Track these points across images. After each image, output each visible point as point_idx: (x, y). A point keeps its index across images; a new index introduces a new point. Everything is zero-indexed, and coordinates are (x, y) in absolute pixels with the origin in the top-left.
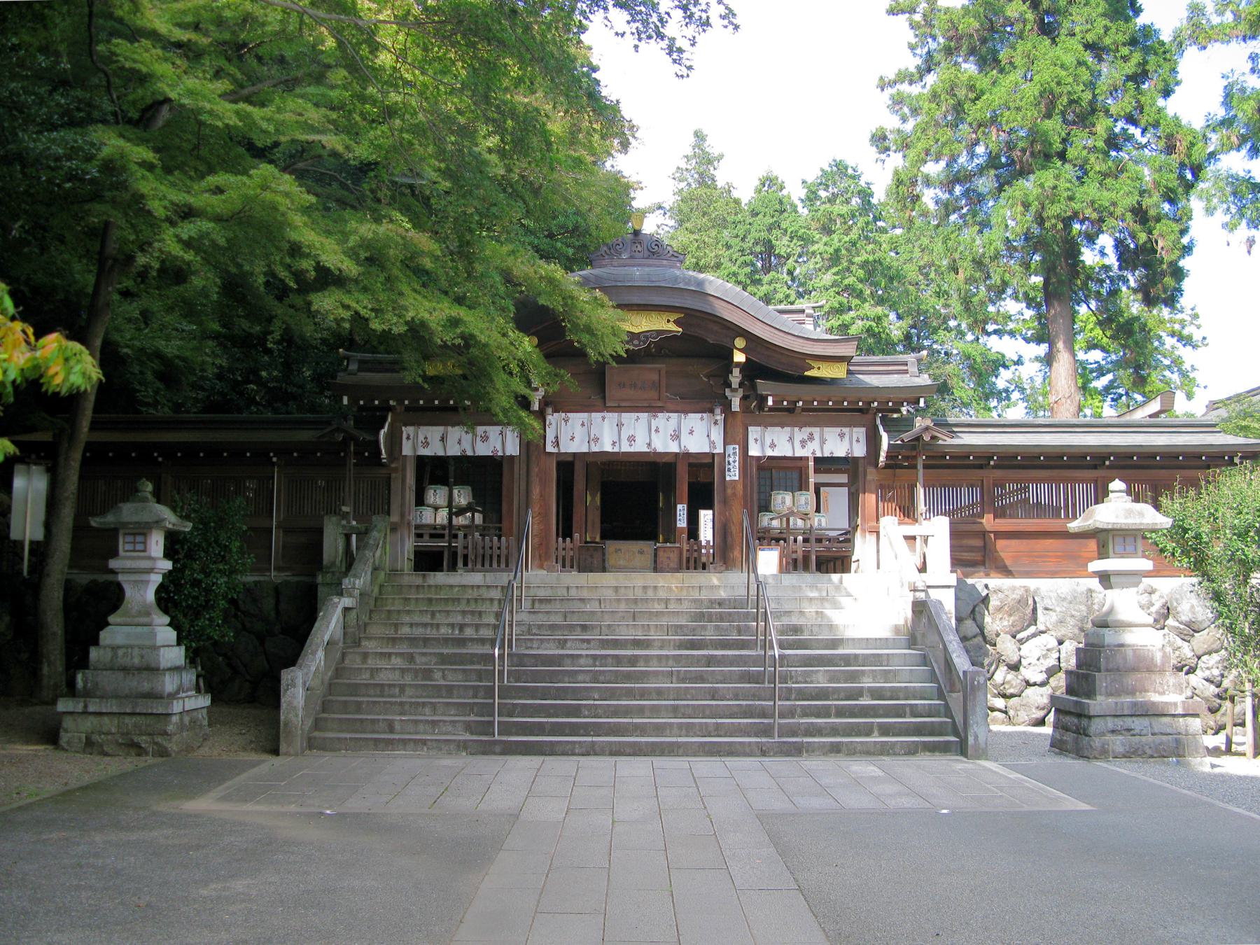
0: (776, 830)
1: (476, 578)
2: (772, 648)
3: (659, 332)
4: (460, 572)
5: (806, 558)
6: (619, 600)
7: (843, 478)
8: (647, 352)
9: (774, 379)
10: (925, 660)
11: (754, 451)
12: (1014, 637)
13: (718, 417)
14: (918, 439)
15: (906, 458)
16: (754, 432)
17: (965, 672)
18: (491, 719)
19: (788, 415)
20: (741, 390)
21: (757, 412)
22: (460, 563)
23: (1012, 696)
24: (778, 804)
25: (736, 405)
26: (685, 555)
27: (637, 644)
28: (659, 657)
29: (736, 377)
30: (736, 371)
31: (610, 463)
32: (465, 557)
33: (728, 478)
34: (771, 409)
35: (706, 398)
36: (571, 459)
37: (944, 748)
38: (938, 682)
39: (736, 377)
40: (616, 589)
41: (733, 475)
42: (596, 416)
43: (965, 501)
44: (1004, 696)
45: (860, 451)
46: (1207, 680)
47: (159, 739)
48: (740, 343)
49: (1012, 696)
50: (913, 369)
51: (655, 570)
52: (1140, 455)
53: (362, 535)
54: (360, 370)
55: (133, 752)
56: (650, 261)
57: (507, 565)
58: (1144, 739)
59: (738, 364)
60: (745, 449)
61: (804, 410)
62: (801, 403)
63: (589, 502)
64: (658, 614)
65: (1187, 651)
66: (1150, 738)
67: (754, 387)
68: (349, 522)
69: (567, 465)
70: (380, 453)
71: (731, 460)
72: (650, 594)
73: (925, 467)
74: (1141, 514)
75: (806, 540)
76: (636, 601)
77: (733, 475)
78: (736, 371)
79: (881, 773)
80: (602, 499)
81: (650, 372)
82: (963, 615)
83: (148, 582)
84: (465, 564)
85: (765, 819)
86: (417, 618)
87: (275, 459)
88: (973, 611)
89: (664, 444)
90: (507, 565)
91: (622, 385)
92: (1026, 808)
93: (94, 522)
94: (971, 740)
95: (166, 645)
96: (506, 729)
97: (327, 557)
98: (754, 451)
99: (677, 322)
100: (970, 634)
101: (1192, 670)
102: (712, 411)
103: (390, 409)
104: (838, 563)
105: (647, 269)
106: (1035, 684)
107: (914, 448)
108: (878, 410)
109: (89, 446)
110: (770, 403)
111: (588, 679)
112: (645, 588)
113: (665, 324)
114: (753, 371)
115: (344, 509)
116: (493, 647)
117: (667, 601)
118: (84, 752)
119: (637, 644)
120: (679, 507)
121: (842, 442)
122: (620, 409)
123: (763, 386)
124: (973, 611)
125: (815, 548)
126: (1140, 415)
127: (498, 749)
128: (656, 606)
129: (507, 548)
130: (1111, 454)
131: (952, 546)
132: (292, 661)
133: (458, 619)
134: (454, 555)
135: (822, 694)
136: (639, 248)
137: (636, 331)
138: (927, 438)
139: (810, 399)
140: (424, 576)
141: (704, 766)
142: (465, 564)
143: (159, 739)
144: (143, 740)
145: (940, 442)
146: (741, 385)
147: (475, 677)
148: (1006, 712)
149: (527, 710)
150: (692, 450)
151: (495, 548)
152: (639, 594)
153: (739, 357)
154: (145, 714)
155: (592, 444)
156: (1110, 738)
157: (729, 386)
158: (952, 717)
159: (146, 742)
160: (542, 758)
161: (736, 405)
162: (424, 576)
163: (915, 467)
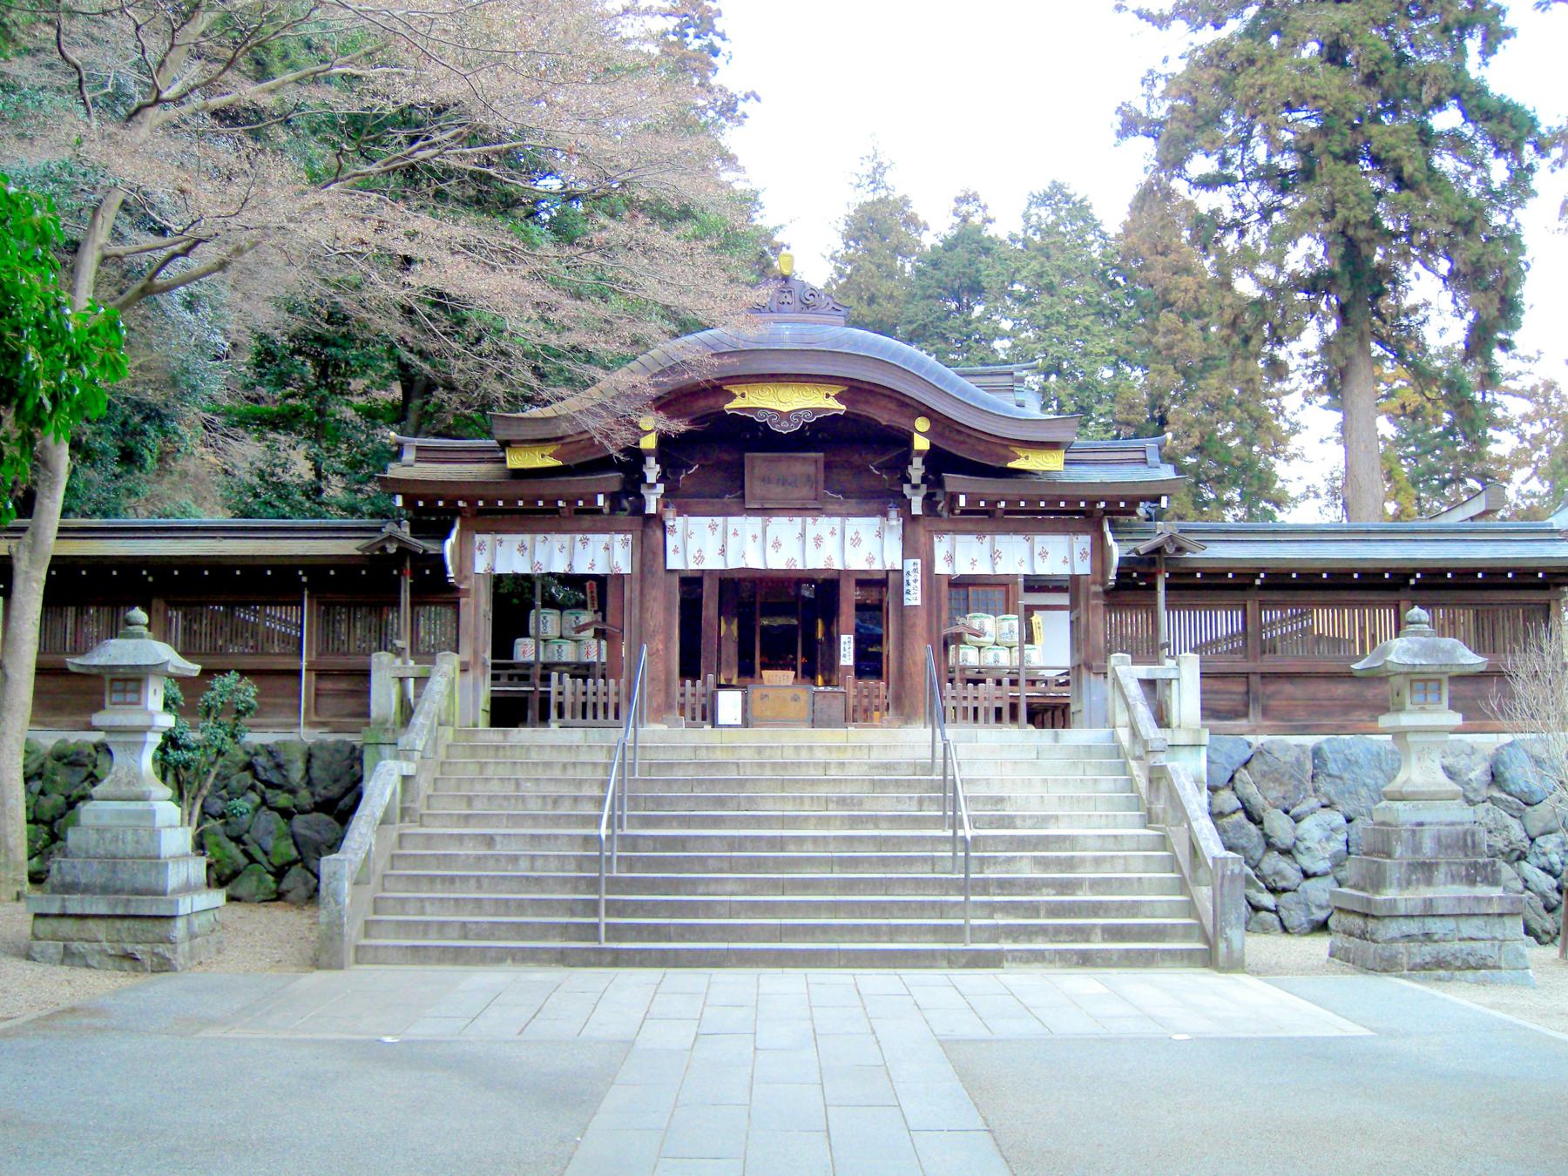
0: (973, 1068)
1: (576, 736)
2: (962, 827)
3: (815, 411)
4: (554, 726)
5: (1014, 708)
6: (761, 765)
7: (1064, 599)
8: (818, 435)
9: (963, 473)
10: (1163, 842)
11: (941, 568)
12: (1287, 812)
13: (894, 523)
14: (1158, 550)
15: (1142, 576)
16: (942, 546)
17: (1214, 858)
18: (603, 928)
19: (985, 518)
20: (924, 487)
21: (943, 513)
22: (554, 713)
23: (1285, 890)
24: (968, 1028)
25: (917, 509)
26: (851, 702)
27: (784, 822)
28: (815, 839)
29: (916, 470)
30: (917, 462)
31: (761, 580)
32: (560, 707)
33: (907, 603)
34: (964, 512)
35: (881, 497)
36: (835, 576)
37: (1188, 958)
38: (1181, 871)
39: (916, 470)
40: (760, 750)
41: (914, 597)
42: (734, 522)
43: (1222, 631)
44: (1273, 891)
45: (1083, 568)
46: (1543, 869)
47: (161, 949)
48: (922, 424)
49: (1285, 890)
50: (1153, 458)
51: (814, 723)
52: (1456, 572)
53: (421, 681)
54: (418, 460)
55: (127, 964)
56: (803, 317)
57: (617, 716)
58: (1448, 946)
59: (920, 453)
60: (929, 565)
61: (1007, 512)
62: (1003, 504)
63: (722, 631)
64: (813, 782)
65: (1516, 832)
66: (1457, 945)
67: (940, 483)
68: (405, 662)
69: (691, 583)
70: (446, 571)
71: (911, 579)
72: (804, 756)
73: (1168, 587)
74: (1450, 653)
75: (1014, 683)
76: (784, 765)
77: (914, 597)
78: (917, 462)
79: (1105, 990)
80: (739, 628)
81: (806, 465)
82: (1219, 784)
83: (144, 743)
84: (561, 715)
85: (948, 1045)
86: (495, 788)
87: (304, 579)
88: (1232, 779)
89: (816, 560)
90: (617, 716)
91: (766, 480)
92: (1298, 1034)
93: (74, 662)
94: (1222, 946)
95: (172, 827)
96: (615, 932)
97: (375, 711)
98: (941, 568)
99: (838, 398)
100: (1227, 809)
101: (1522, 857)
102: (885, 514)
103: (458, 512)
104: (1058, 713)
105: (798, 326)
106: (1315, 875)
107: (1152, 562)
108: (1105, 512)
109: (58, 563)
110: (962, 501)
111: (711, 862)
112: (797, 748)
113: (823, 401)
114: (939, 462)
115: (399, 643)
116: (598, 826)
117: (826, 766)
118: (62, 963)
119: (784, 822)
120: (844, 638)
121: (1060, 554)
122: (764, 511)
123: (952, 481)
124: (1232, 779)
125: (1024, 693)
126: (1456, 518)
127: (609, 958)
128: (812, 771)
129: (617, 694)
130: (1417, 570)
131: (1203, 692)
132: (334, 846)
133: (552, 790)
134: (545, 701)
135: (1031, 886)
136: (789, 299)
137: (785, 409)
138: (1170, 550)
139: (994, 498)
140: (505, 734)
141: (875, 980)
142: (561, 715)
143: (161, 949)
144: (139, 949)
145: (1188, 555)
146: (924, 479)
147: (573, 866)
148: (1276, 912)
149: (629, 907)
150: (853, 568)
151: (600, 693)
152: (790, 756)
153: (921, 444)
154: (149, 917)
155: (1037, 559)
156: (1400, 946)
157: (909, 481)
158: (1199, 918)
159: (144, 952)
160: (663, 970)
161: (917, 509)
162: (505, 734)
163: (1152, 587)
